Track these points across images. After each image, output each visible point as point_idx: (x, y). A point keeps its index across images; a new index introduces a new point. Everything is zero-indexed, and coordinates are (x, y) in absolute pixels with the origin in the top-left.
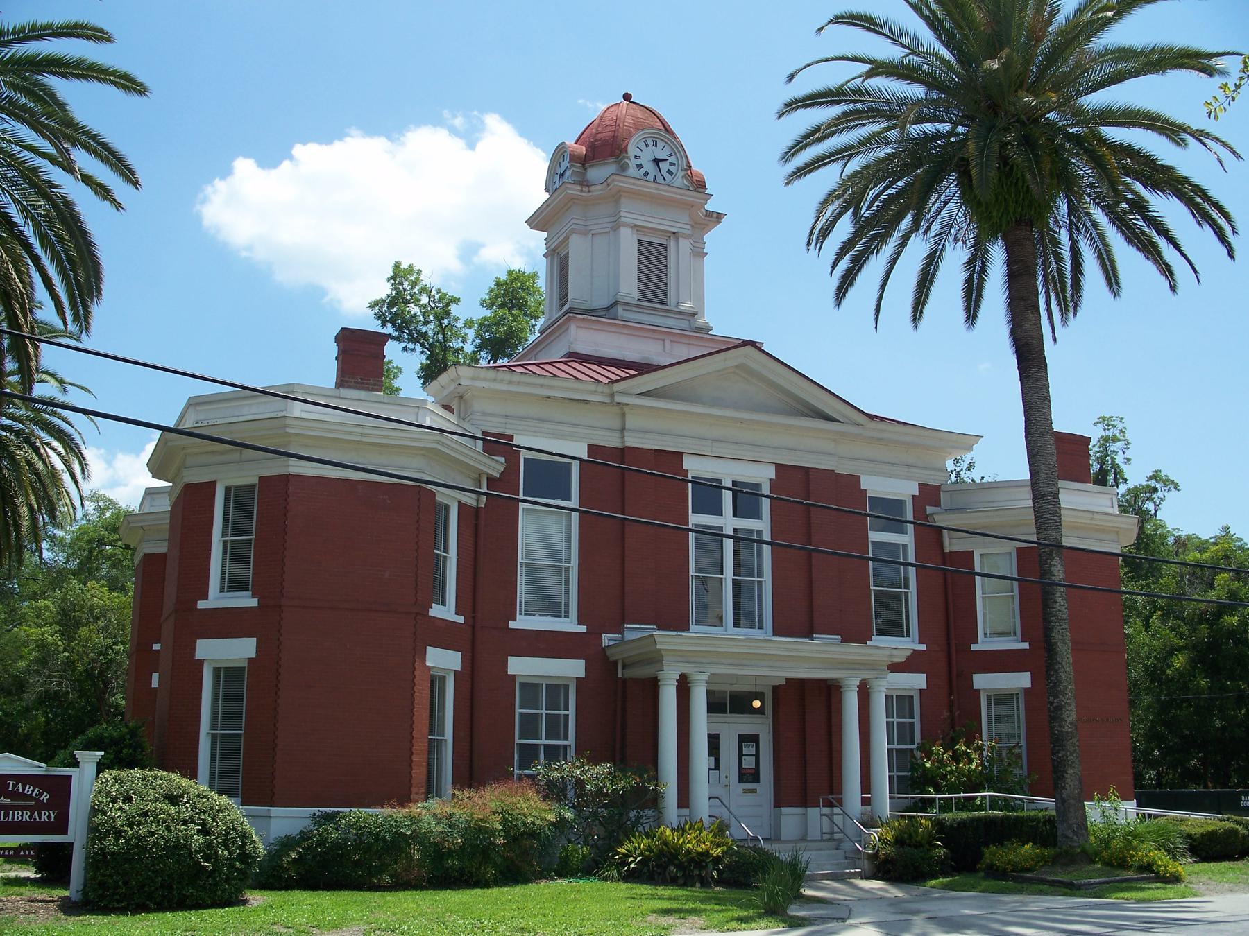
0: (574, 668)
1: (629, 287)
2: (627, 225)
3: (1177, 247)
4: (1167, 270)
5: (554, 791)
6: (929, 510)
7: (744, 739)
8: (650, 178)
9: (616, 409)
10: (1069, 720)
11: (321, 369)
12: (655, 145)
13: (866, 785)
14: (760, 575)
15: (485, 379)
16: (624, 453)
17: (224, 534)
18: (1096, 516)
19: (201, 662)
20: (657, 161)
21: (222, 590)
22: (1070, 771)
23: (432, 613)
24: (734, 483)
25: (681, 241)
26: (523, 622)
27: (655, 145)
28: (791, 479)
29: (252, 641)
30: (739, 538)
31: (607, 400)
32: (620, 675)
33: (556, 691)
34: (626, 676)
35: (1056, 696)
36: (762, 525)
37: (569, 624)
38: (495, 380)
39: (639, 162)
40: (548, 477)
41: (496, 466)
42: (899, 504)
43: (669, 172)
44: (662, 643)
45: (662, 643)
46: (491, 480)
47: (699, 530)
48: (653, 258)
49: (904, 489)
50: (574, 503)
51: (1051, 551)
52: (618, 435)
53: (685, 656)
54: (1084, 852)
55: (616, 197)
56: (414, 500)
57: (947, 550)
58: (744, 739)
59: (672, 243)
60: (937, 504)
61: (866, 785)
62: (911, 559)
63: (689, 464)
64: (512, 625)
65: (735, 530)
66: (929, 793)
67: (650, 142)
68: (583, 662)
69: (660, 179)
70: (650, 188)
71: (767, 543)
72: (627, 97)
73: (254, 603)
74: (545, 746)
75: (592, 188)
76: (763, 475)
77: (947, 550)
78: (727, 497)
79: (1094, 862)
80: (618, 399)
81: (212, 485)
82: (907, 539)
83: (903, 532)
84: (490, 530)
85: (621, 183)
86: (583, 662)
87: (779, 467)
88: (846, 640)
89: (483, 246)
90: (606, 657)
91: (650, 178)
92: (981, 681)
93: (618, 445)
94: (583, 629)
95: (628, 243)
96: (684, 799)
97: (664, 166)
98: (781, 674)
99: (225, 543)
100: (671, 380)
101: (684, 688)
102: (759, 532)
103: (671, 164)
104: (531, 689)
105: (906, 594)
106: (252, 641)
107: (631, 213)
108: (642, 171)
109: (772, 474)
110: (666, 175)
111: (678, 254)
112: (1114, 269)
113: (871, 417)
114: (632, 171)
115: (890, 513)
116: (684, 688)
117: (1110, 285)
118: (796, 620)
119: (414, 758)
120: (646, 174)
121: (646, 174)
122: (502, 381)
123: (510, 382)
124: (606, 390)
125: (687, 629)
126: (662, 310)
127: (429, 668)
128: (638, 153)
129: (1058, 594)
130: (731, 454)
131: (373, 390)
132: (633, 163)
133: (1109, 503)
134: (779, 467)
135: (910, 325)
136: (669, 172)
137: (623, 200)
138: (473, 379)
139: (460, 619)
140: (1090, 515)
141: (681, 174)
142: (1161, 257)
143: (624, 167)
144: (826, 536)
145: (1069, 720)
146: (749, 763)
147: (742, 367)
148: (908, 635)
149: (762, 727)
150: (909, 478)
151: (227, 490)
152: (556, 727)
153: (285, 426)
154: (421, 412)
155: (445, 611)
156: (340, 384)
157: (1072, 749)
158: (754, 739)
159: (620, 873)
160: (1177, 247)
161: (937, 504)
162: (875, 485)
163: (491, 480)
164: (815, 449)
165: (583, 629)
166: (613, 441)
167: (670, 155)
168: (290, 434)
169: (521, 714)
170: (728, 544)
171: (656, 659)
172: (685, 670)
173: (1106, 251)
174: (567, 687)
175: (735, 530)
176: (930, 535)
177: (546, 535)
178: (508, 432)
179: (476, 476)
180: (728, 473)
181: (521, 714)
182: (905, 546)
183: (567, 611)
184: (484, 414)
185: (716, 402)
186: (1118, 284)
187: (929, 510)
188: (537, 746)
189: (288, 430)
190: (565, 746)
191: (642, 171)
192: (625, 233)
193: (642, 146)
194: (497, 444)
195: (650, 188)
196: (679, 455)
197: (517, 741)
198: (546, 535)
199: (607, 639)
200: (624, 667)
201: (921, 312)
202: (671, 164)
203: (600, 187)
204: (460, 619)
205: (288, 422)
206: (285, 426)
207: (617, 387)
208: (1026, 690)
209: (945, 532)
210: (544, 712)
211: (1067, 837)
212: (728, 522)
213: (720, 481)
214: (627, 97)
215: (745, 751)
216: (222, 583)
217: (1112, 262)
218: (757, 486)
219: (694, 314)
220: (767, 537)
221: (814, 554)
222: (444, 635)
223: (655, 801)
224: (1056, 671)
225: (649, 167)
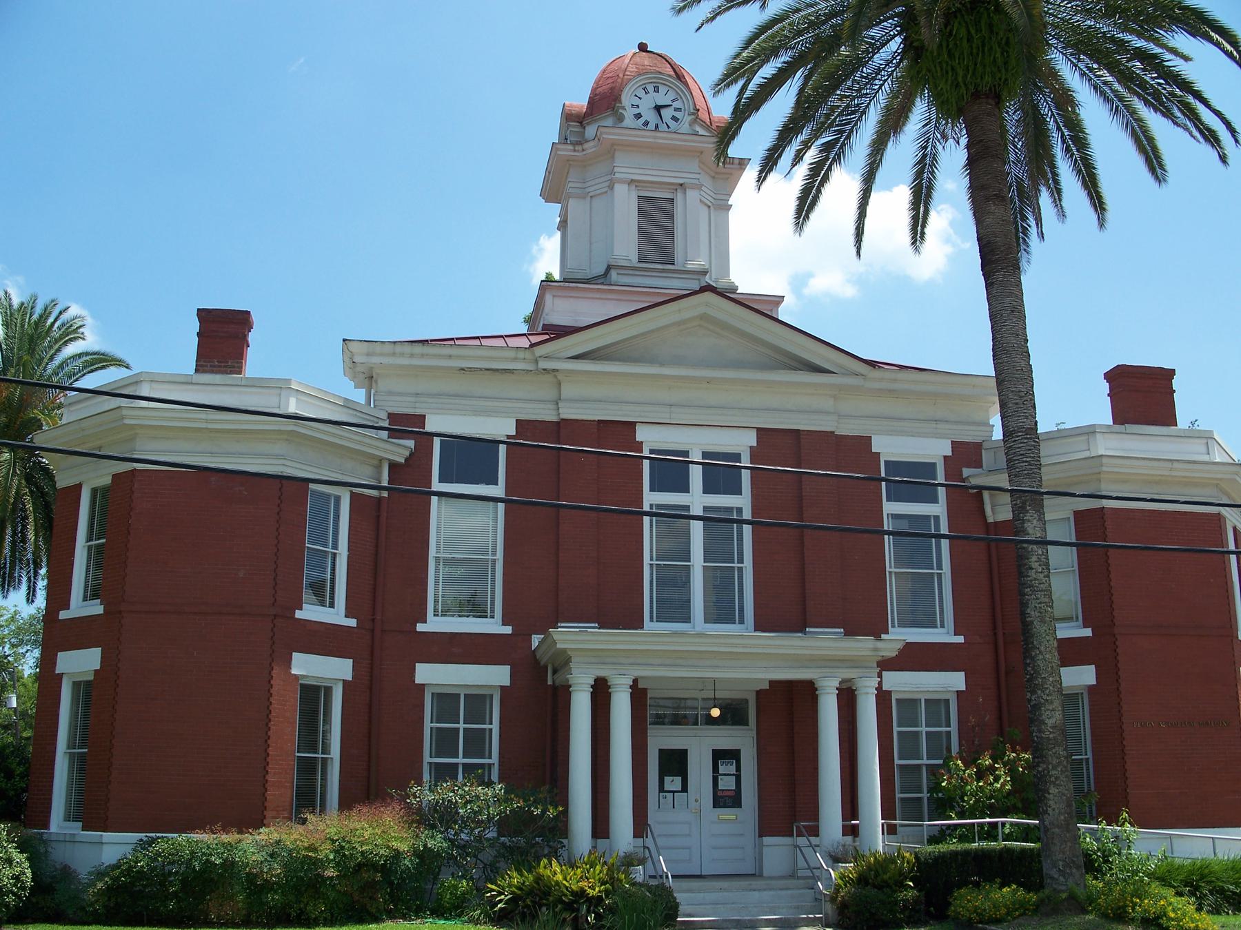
0: (497, 676)
1: (626, 247)
2: (622, 181)
3: (1205, 102)
4: (1211, 137)
5: (422, 818)
6: (966, 472)
7: (719, 756)
8: (651, 126)
9: (549, 378)
10: (1050, 722)
11: (181, 350)
12: (657, 90)
13: (851, 806)
14: (741, 561)
15: (382, 355)
16: (561, 428)
17: (89, 539)
18: (1176, 465)
19: (60, 676)
20: (658, 108)
21: (85, 599)
22: (1053, 790)
23: (299, 614)
24: (705, 455)
25: (689, 193)
26: (434, 624)
27: (657, 90)
28: (772, 442)
29: (506, 669)
30: (716, 521)
31: (530, 367)
32: (550, 682)
33: (477, 702)
34: (557, 683)
35: (1033, 692)
36: (742, 502)
37: (493, 626)
38: (394, 354)
39: (636, 111)
40: (470, 457)
41: (401, 449)
42: (930, 468)
43: (675, 119)
44: (564, 641)
45: (564, 641)
46: (393, 466)
47: (660, 514)
48: (657, 218)
49: (934, 450)
50: (498, 490)
51: (1024, 503)
52: (554, 407)
53: (599, 656)
54: (1072, 897)
55: (610, 151)
56: (287, 492)
57: (991, 520)
58: (719, 756)
59: (679, 196)
60: (979, 464)
61: (851, 806)
62: (944, 530)
63: (642, 434)
64: (420, 627)
65: (706, 509)
66: (950, 818)
67: (650, 88)
68: (508, 667)
69: (663, 127)
70: (647, 137)
71: (944, 536)
72: (643, 47)
73: (1090, 634)
74: (464, 765)
75: (586, 146)
76: (742, 442)
77: (991, 520)
78: (696, 474)
79: (1087, 912)
80: (543, 364)
81: (79, 487)
82: (937, 509)
83: (935, 500)
84: (392, 524)
85: (612, 135)
86: (508, 667)
87: (761, 432)
88: (849, 633)
89: (810, 275)
90: (537, 662)
91: (651, 126)
92: (426, 673)
93: (554, 418)
94: (508, 630)
95: (625, 204)
96: (601, 827)
97: (667, 114)
98: (764, 675)
99: (90, 548)
100: (609, 340)
101: (601, 693)
102: (740, 510)
103: (676, 110)
104: (447, 701)
105: (940, 575)
106: (506, 669)
107: (625, 167)
108: (642, 121)
109: (751, 439)
110: (672, 123)
111: (690, 212)
112: (1155, 149)
113: (872, 364)
114: (629, 121)
115: (912, 480)
116: (601, 693)
117: (1152, 170)
118: (783, 612)
119: (270, 778)
120: (646, 123)
121: (646, 123)
122: (402, 354)
123: (412, 356)
124: (528, 355)
125: (640, 625)
126: (663, 271)
127: (297, 677)
128: (636, 101)
129: (1034, 558)
130: (697, 421)
131: (231, 373)
132: (629, 114)
133: (1203, 449)
134: (761, 432)
135: (910, 249)
136: (675, 119)
137: (617, 154)
138: (368, 355)
139: (353, 623)
140: (1169, 465)
141: (688, 119)
142: (1200, 120)
143: (621, 119)
144: (817, 514)
145: (1050, 722)
146: (727, 783)
147: (704, 317)
148: (942, 626)
149: (742, 739)
150: (259, 384)
151: (94, 491)
152: (476, 743)
153: (123, 418)
154: (284, 393)
155: (335, 614)
156: (197, 371)
157: (1055, 761)
158: (733, 755)
159: (487, 915)
160: (1205, 102)
161: (979, 464)
162: (890, 447)
163: (393, 466)
164: (806, 408)
165: (508, 630)
166: (546, 414)
167: (676, 100)
168: (132, 427)
169: (899, 733)
170: (697, 528)
171: (562, 662)
172: (602, 673)
173: (1141, 127)
174: (328, 690)
175: (706, 509)
176: (967, 501)
177: (465, 528)
178: (419, 411)
179: (376, 462)
180: (696, 443)
181: (899, 733)
182: (937, 518)
183: (493, 611)
184: (390, 393)
185: (678, 361)
186: (1161, 166)
187: (966, 472)
188: (919, 767)
189: (127, 421)
190: (490, 765)
191: (642, 121)
192: (621, 190)
193: (641, 93)
194: (405, 425)
195: (647, 137)
196: (632, 425)
197: (897, 762)
198: (465, 528)
199: (536, 640)
200: (555, 672)
201: (923, 234)
202: (676, 110)
203: (592, 144)
204: (353, 623)
205: (125, 412)
206: (123, 418)
207: (540, 351)
208: (1090, 688)
209: (986, 494)
210: (461, 726)
211: (1052, 878)
212: (697, 499)
213: (686, 453)
214: (643, 47)
215: (722, 769)
216: (86, 591)
217: (1150, 140)
218: (737, 457)
219: (704, 273)
220: (747, 515)
221: (1111, 551)
222: (324, 640)
223: (560, 828)
224: (1033, 658)
225: (650, 116)
